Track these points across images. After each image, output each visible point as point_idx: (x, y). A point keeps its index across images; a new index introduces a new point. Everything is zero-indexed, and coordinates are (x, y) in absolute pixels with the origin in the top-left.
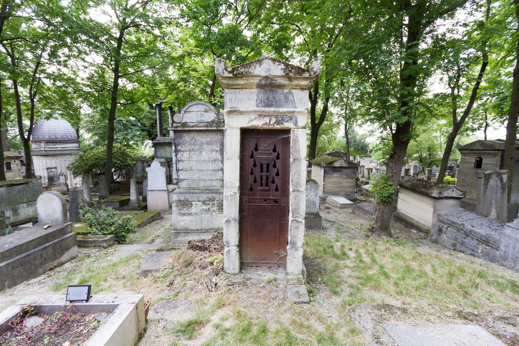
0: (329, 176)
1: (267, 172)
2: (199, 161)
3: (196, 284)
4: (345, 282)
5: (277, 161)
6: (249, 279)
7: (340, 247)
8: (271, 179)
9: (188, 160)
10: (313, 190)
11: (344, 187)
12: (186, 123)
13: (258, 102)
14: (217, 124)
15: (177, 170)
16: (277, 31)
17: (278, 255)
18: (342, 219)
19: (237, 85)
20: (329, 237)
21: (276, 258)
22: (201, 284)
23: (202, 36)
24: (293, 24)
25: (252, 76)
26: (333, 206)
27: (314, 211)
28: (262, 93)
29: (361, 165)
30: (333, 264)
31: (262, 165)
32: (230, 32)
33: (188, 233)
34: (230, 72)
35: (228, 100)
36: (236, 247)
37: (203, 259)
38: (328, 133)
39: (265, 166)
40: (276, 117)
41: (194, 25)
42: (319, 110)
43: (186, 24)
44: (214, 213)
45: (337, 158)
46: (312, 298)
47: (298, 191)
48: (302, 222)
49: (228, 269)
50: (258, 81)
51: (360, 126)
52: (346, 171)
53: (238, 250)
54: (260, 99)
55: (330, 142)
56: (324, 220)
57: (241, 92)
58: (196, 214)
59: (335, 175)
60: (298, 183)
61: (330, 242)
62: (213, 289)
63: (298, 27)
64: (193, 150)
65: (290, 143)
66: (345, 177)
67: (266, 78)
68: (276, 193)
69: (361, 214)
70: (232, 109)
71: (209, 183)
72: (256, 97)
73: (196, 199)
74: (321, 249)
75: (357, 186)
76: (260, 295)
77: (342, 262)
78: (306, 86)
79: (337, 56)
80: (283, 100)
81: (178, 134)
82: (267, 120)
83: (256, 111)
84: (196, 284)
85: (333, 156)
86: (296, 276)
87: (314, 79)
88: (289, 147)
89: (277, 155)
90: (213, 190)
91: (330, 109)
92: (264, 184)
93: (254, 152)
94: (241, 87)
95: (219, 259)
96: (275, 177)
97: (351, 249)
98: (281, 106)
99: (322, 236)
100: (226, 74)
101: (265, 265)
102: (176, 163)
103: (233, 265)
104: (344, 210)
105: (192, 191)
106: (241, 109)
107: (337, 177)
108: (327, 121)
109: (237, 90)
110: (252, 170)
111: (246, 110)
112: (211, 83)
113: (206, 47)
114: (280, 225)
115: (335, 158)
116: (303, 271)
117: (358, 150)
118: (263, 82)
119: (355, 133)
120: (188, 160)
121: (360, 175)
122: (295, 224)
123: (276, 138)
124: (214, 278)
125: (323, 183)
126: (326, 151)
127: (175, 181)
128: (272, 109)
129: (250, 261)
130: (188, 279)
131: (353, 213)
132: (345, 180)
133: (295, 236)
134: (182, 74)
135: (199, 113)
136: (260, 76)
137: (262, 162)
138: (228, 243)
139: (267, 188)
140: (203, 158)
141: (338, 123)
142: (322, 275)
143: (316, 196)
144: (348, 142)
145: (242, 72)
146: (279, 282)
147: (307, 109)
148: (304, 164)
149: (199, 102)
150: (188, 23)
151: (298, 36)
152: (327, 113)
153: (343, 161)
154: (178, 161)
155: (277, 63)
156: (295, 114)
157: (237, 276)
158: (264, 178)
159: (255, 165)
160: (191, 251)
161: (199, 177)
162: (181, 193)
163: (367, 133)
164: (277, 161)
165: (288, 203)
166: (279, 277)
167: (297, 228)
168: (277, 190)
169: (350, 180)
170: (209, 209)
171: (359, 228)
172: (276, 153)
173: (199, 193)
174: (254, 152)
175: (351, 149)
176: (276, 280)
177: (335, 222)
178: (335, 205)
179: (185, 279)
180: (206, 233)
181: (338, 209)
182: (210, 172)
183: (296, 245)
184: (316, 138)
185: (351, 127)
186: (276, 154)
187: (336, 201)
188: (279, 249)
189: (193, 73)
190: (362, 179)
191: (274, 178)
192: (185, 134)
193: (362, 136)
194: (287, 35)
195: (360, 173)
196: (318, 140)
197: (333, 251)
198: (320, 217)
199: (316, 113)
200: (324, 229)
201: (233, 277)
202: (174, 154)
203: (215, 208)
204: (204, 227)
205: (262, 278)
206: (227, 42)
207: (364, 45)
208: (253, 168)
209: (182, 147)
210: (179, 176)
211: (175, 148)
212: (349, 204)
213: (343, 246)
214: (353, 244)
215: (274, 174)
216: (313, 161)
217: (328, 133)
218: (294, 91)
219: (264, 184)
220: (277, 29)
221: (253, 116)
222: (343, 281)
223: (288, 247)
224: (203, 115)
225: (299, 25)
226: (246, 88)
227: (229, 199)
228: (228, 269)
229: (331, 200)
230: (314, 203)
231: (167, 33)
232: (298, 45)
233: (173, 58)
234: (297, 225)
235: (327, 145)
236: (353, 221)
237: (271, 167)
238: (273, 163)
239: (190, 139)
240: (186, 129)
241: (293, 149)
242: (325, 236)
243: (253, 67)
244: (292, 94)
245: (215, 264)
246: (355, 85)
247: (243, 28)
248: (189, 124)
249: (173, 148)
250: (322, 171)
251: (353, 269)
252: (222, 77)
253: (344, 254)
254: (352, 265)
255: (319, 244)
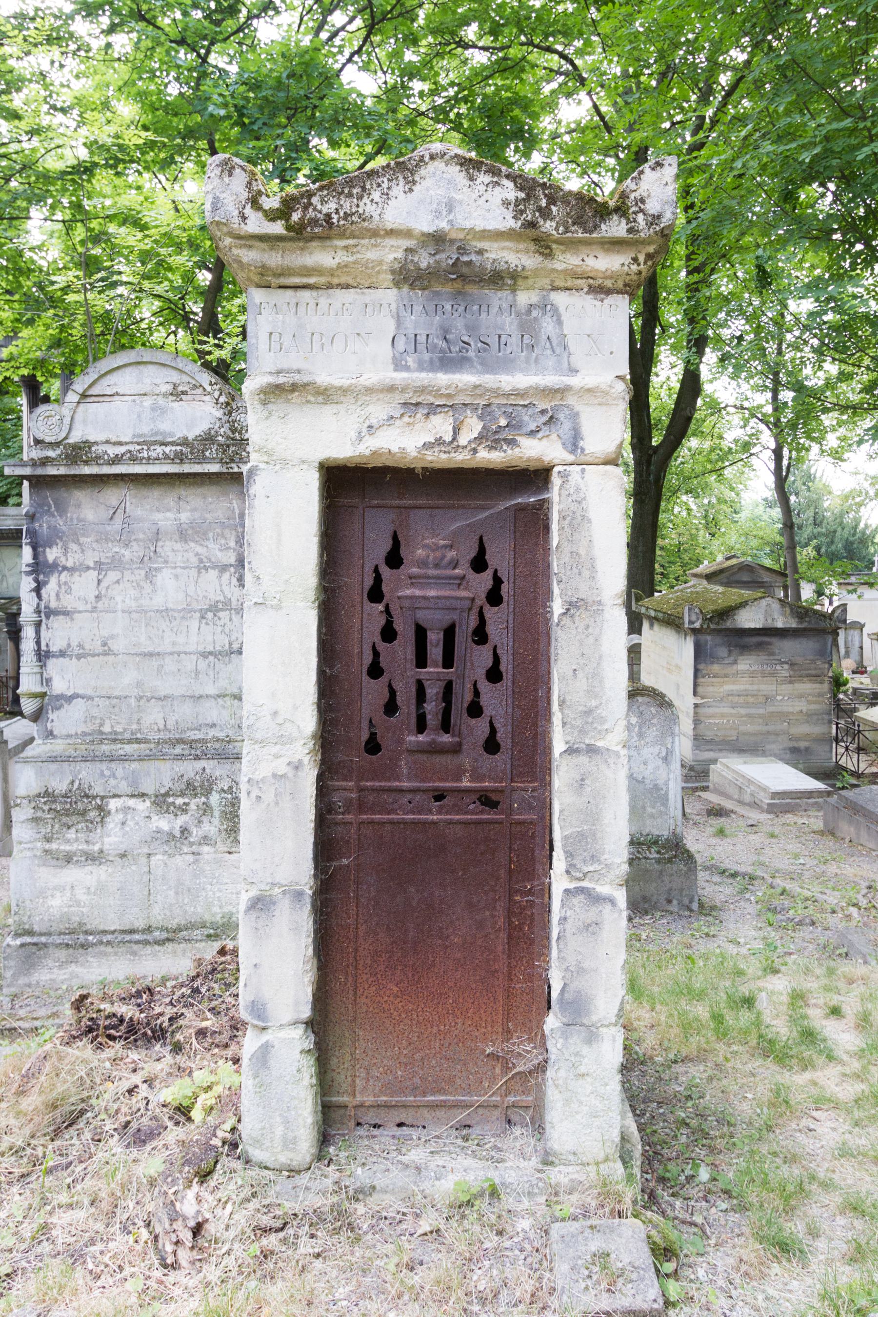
0: (716, 668)
1: (448, 662)
2: (142, 611)
3: (100, 1226)
4: (826, 1185)
5: (490, 613)
6: (360, 1194)
7: (785, 999)
8: (463, 697)
9: (94, 609)
10: (652, 733)
11: (783, 716)
12: (87, 445)
13: (401, 345)
14: (224, 448)
15: (42, 656)
16: (483, 75)
17: (503, 1061)
18: (784, 863)
19: (308, 271)
20: (732, 949)
21: (493, 1080)
22: (126, 1230)
23: (174, 90)
24: (549, 50)
25: (374, 233)
26: (741, 802)
27: (661, 829)
28: (418, 308)
29: (850, 618)
30: (763, 1091)
31: (421, 633)
32: (292, 75)
33: (84, 946)
34: (272, 216)
35: (263, 337)
36: (300, 1029)
37: (144, 1088)
38: (706, 487)
39: (435, 638)
40: (486, 412)
41: (137, 48)
42: (663, 393)
43: (103, 40)
44: (206, 849)
45: (746, 593)
46: (674, 1289)
47: (592, 750)
48: (612, 901)
49: (257, 1143)
50: (400, 254)
51: (837, 456)
52: (788, 647)
53: (309, 1043)
54: (411, 332)
55: (712, 525)
56: (706, 868)
57: (323, 301)
58: (123, 856)
59: (745, 664)
60: (589, 712)
61: (740, 973)
62: (184, 1256)
63: (572, 63)
64: (116, 563)
65: (547, 528)
66: (784, 671)
67: (438, 239)
68: (488, 761)
69: (864, 838)
70: (281, 380)
71: (184, 713)
72: (390, 327)
73: (124, 787)
74: (702, 1011)
75: (840, 710)
76: (415, 1279)
77: (802, 1078)
78: (613, 276)
79: (739, 164)
80: (515, 340)
81: (49, 496)
82: (442, 426)
83: (392, 389)
84: (100, 1226)
85: (728, 584)
86: (592, 1169)
87: (651, 249)
88: (547, 550)
89: (490, 584)
90: (204, 741)
91: (708, 388)
92: (432, 720)
93: (385, 571)
94: (322, 280)
95: (218, 1090)
96: (485, 686)
97: (835, 1011)
98: (506, 365)
99: (703, 946)
100: (256, 224)
101: (440, 1113)
102: (38, 625)
103: (286, 1122)
104: (789, 818)
105: (106, 748)
106: (323, 379)
107: (752, 675)
108: (697, 433)
109: (306, 294)
110: (376, 653)
111: (345, 383)
112: (205, 278)
113: (190, 133)
114: (510, 914)
115: (736, 594)
116: (624, 1138)
117: (833, 557)
118: (424, 260)
119: (818, 484)
120: (94, 609)
121: (847, 665)
122: (578, 908)
123: (483, 508)
124: (191, 1194)
125: (691, 700)
126: (699, 562)
127: (28, 706)
128: (466, 378)
129: (369, 1099)
130: (64, 1198)
131: (830, 832)
132: (787, 688)
133: (581, 971)
134: (83, 242)
135: (148, 402)
136: (407, 233)
137: (422, 616)
138: (258, 1009)
139: (446, 738)
140: (158, 601)
141: (746, 446)
142: (712, 1150)
143: (666, 759)
144: (789, 526)
145: (328, 216)
146: (508, 1201)
147: (620, 378)
148: (619, 619)
149: (147, 356)
150: (113, 38)
151: (569, 95)
152: (699, 402)
153: (776, 606)
154: (45, 613)
155: (484, 178)
156: (571, 400)
157: (304, 1179)
158: (433, 691)
159: (389, 633)
160: (83, 1050)
161: (139, 684)
162: (53, 759)
163: (866, 485)
164: (490, 613)
165: (545, 808)
166: (511, 1177)
167: (591, 928)
168: (492, 746)
169: (807, 687)
170: (184, 831)
171: (863, 903)
172: (487, 575)
173: (140, 759)
174: (385, 571)
175: (805, 554)
176: (494, 1193)
177: (752, 878)
178: (747, 798)
179: (45, 1201)
180: (170, 946)
181: (764, 817)
182: (189, 663)
183: (588, 1013)
184: (658, 506)
185: (799, 460)
186: (485, 580)
187: (750, 782)
188: (508, 1034)
189: (123, 230)
190: (856, 682)
191: (477, 693)
192: (80, 496)
193: (846, 498)
194: (526, 91)
195: (847, 655)
196: (662, 517)
197: (758, 1023)
198: (689, 857)
199: (653, 403)
200: (707, 910)
201: (283, 1184)
202: (27, 584)
203: (212, 827)
204: (158, 915)
205: (426, 1185)
206: (273, 115)
207: (848, 122)
208: (382, 646)
209: (66, 553)
210: (49, 681)
211: (35, 556)
212: (810, 794)
213: (798, 997)
214: (842, 985)
215: (480, 674)
216: (647, 606)
217: (706, 487)
218: (560, 299)
219: (432, 720)
220: (484, 68)
221: (378, 411)
222: (813, 1178)
223: (552, 1022)
224: (163, 411)
225: (570, 51)
226: (348, 287)
227: (269, 796)
228: (257, 1143)
229: (730, 776)
230: (658, 794)
231: (22, 80)
232: (569, 132)
233: (46, 177)
234: (591, 915)
235: (703, 535)
236: (832, 869)
237: (463, 637)
238: (473, 622)
239: (105, 514)
240: (87, 470)
241: (566, 558)
242: (711, 946)
243: (376, 195)
244: (556, 311)
245: (197, 1114)
246: (813, 287)
247: (342, 59)
248: (101, 448)
249: (27, 553)
250: (687, 648)
251: (857, 1114)
252: (239, 237)
253: (809, 1035)
254: (848, 1091)
255: (690, 990)
